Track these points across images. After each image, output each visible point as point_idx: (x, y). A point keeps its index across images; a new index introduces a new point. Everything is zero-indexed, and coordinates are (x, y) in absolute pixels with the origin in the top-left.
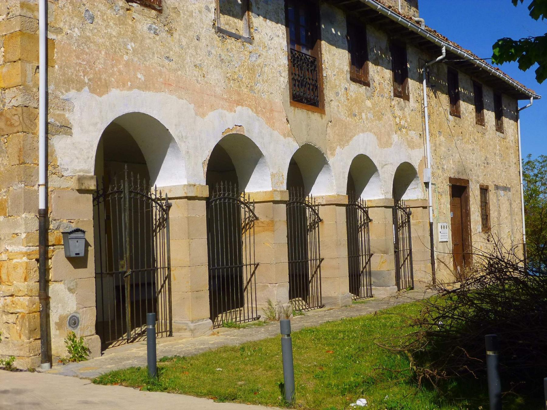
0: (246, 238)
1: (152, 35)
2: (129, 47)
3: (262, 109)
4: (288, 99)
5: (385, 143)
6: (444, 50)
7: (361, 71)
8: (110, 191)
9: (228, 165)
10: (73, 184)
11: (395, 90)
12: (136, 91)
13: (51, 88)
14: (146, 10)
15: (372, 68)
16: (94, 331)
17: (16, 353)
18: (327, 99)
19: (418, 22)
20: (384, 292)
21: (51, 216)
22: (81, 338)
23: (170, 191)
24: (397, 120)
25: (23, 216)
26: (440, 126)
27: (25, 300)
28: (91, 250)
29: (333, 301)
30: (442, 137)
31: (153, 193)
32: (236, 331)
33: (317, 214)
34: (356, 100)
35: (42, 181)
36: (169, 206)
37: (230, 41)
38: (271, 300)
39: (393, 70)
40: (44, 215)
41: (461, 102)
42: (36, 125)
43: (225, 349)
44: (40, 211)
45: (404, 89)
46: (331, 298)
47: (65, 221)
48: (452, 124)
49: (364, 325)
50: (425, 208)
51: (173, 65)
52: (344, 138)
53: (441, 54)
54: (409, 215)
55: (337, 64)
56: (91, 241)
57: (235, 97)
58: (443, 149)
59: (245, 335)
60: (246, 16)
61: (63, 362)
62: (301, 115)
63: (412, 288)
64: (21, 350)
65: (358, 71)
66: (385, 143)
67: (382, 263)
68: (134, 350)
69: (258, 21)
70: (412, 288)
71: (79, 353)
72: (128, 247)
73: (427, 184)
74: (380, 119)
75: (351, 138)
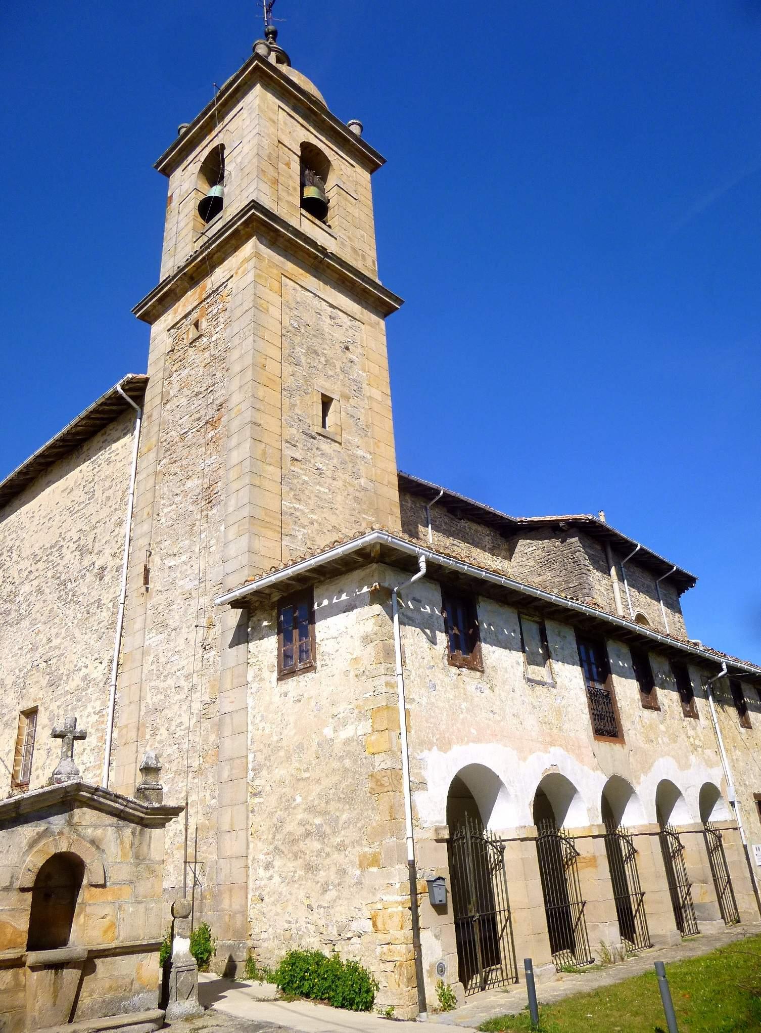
0: (569, 874)
1: (479, 693)
2: (463, 707)
3: (572, 747)
4: (591, 734)
5: (684, 766)
6: (724, 666)
7: (650, 696)
8: (455, 838)
9: (549, 803)
10: (431, 835)
11: (684, 710)
12: (471, 744)
13: (410, 750)
14: (473, 673)
15: (659, 692)
16: (458, 979)
17: (395, 1002)
18: (625, 729)
19: (695, 644)
20: (712, 927)
21: (417, 866)
22: (449, 986)
23: (503, 833)
24: (692, 740)
25: (397, 867)
26: (734, 739)
27: (402, 948)
28: (450, 895)
29: (663, 940)
30: (737, 752)
31: (486, 835)
32: (577, 975)
33: (631, 845)
34: (651, 725)
35: (409, 834)
36: (503, 848)
37: (539, 688)
38: (604, 939)
39: (679, 691)
40: (412, 865)
41: (749, 712)
42: (401, 784)
43: (580, 995)
44: (409, 861)
45: (692, 708)
46: (658, 936)
47: (428, 870)
48: (744, 737)
49: (707, 967)
50: (735, 829)
51: (497, 717)
52: (646, 766)
53: (722, 670)
54: (719, 837)
55: (628, 695)
56: (449, 890)
57: (548, 739)
58: (741, 764)
59: (588, 981)
60: (547, 664)
61: (435, 1010)
62: (605, 747)
63: (738, 921)
64: (400, 999)
65: (647, 698)
66: (684, 766)
67: (702, 894)
68: (493, 998)
69: (557, 666)
70: (738, 921)
71: (448, 1002)
72: (474, 891)
73: (732, 804)
74: (675, 742)
75: (652, 764)
